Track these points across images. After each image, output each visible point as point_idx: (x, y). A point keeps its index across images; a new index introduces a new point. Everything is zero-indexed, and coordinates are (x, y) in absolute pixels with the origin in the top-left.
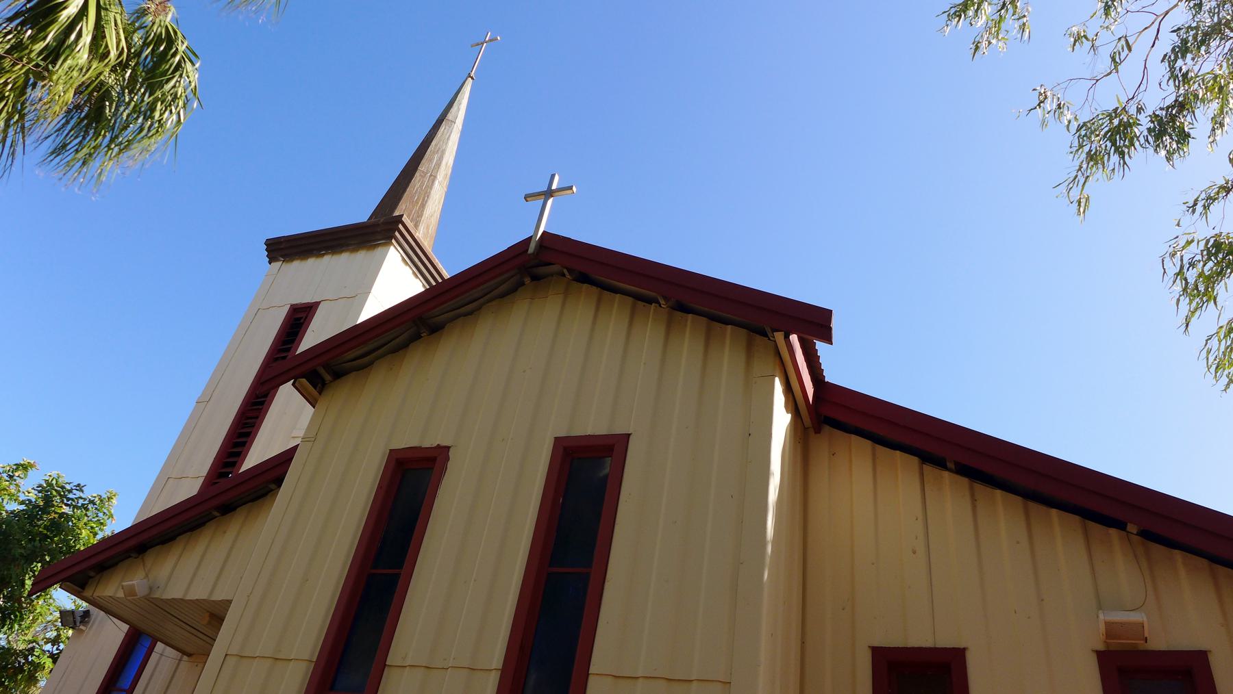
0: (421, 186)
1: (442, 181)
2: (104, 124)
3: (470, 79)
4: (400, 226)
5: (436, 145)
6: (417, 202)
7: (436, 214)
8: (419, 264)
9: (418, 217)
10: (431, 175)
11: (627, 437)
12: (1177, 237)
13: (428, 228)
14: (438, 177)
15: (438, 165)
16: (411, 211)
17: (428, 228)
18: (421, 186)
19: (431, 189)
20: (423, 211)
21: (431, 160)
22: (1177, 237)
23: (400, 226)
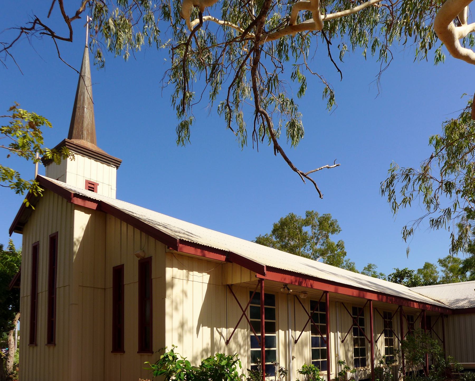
0: (80, 114)
1: (88, 107)
2: (442, 56)
3: (86, 48)
4: (67, 143)
5: (81, 91)
6: (80, 122)
7: (90, 123)
8: (82, 152)
9: (82, 129)
10: (82, 107)
11: (123, 265)
12: (399, 41)
13: (88, 130)
14: (85, 106)
15: (84, 100)
16: (79, 127)
17: (88, 130)
18: (80, 114)
19: (84, 113)
20: (83, 125)
21: (80, 100)
22: (399, 41)
23: (67, 143)
